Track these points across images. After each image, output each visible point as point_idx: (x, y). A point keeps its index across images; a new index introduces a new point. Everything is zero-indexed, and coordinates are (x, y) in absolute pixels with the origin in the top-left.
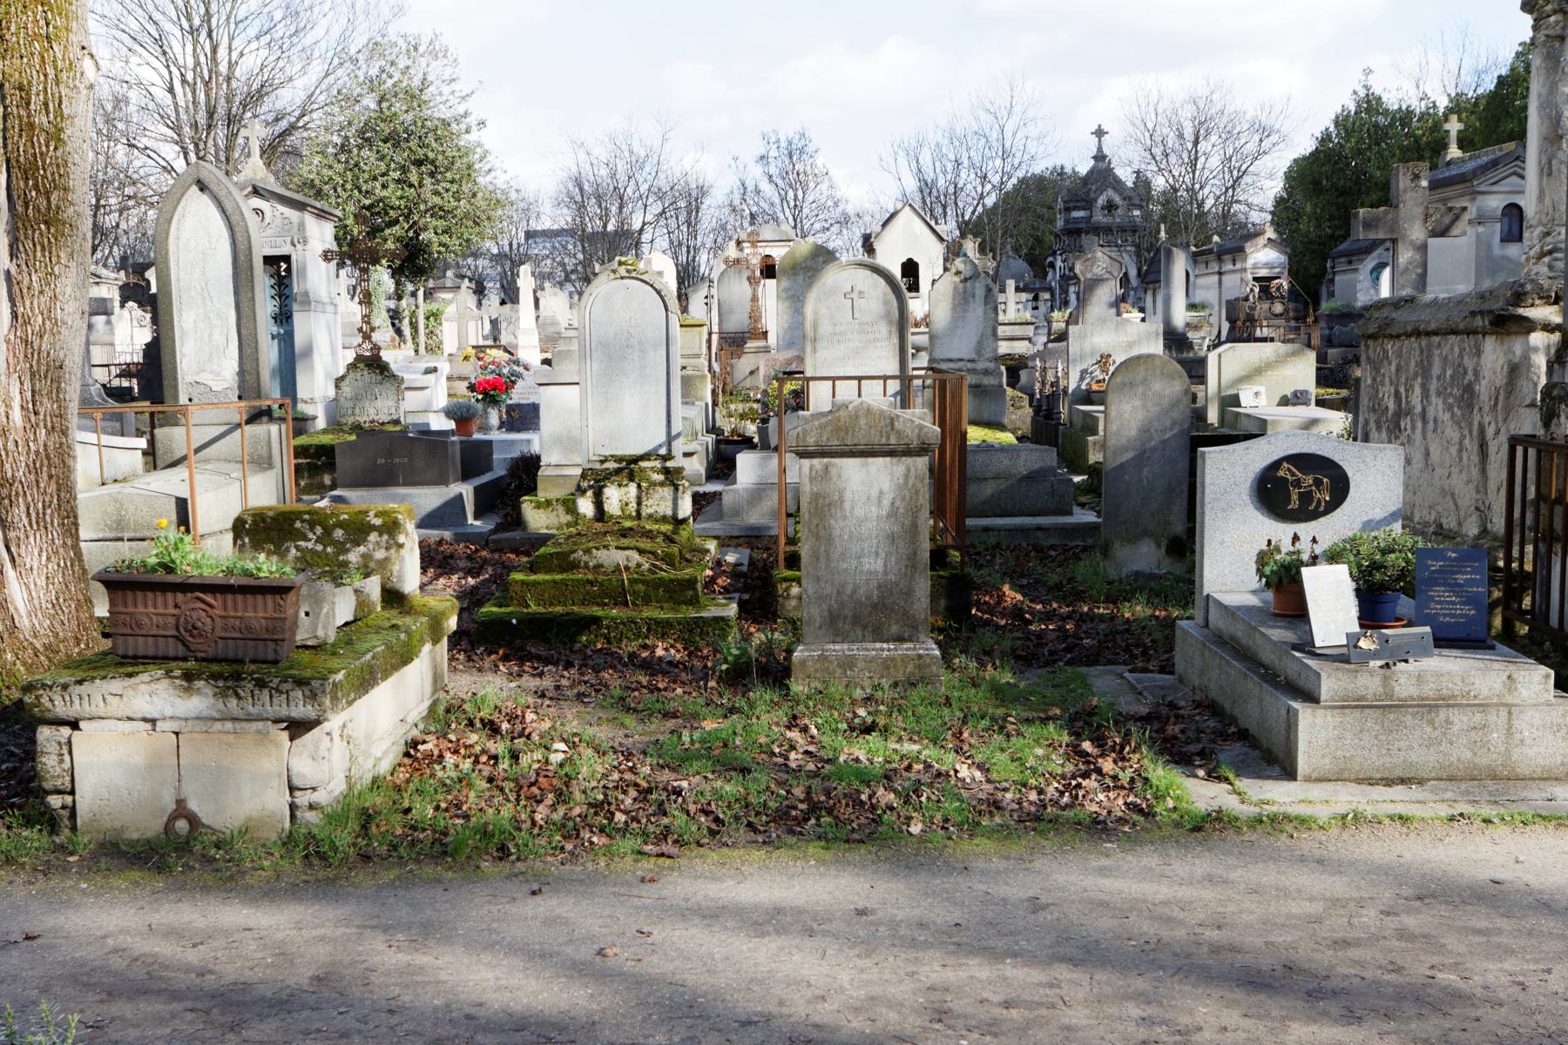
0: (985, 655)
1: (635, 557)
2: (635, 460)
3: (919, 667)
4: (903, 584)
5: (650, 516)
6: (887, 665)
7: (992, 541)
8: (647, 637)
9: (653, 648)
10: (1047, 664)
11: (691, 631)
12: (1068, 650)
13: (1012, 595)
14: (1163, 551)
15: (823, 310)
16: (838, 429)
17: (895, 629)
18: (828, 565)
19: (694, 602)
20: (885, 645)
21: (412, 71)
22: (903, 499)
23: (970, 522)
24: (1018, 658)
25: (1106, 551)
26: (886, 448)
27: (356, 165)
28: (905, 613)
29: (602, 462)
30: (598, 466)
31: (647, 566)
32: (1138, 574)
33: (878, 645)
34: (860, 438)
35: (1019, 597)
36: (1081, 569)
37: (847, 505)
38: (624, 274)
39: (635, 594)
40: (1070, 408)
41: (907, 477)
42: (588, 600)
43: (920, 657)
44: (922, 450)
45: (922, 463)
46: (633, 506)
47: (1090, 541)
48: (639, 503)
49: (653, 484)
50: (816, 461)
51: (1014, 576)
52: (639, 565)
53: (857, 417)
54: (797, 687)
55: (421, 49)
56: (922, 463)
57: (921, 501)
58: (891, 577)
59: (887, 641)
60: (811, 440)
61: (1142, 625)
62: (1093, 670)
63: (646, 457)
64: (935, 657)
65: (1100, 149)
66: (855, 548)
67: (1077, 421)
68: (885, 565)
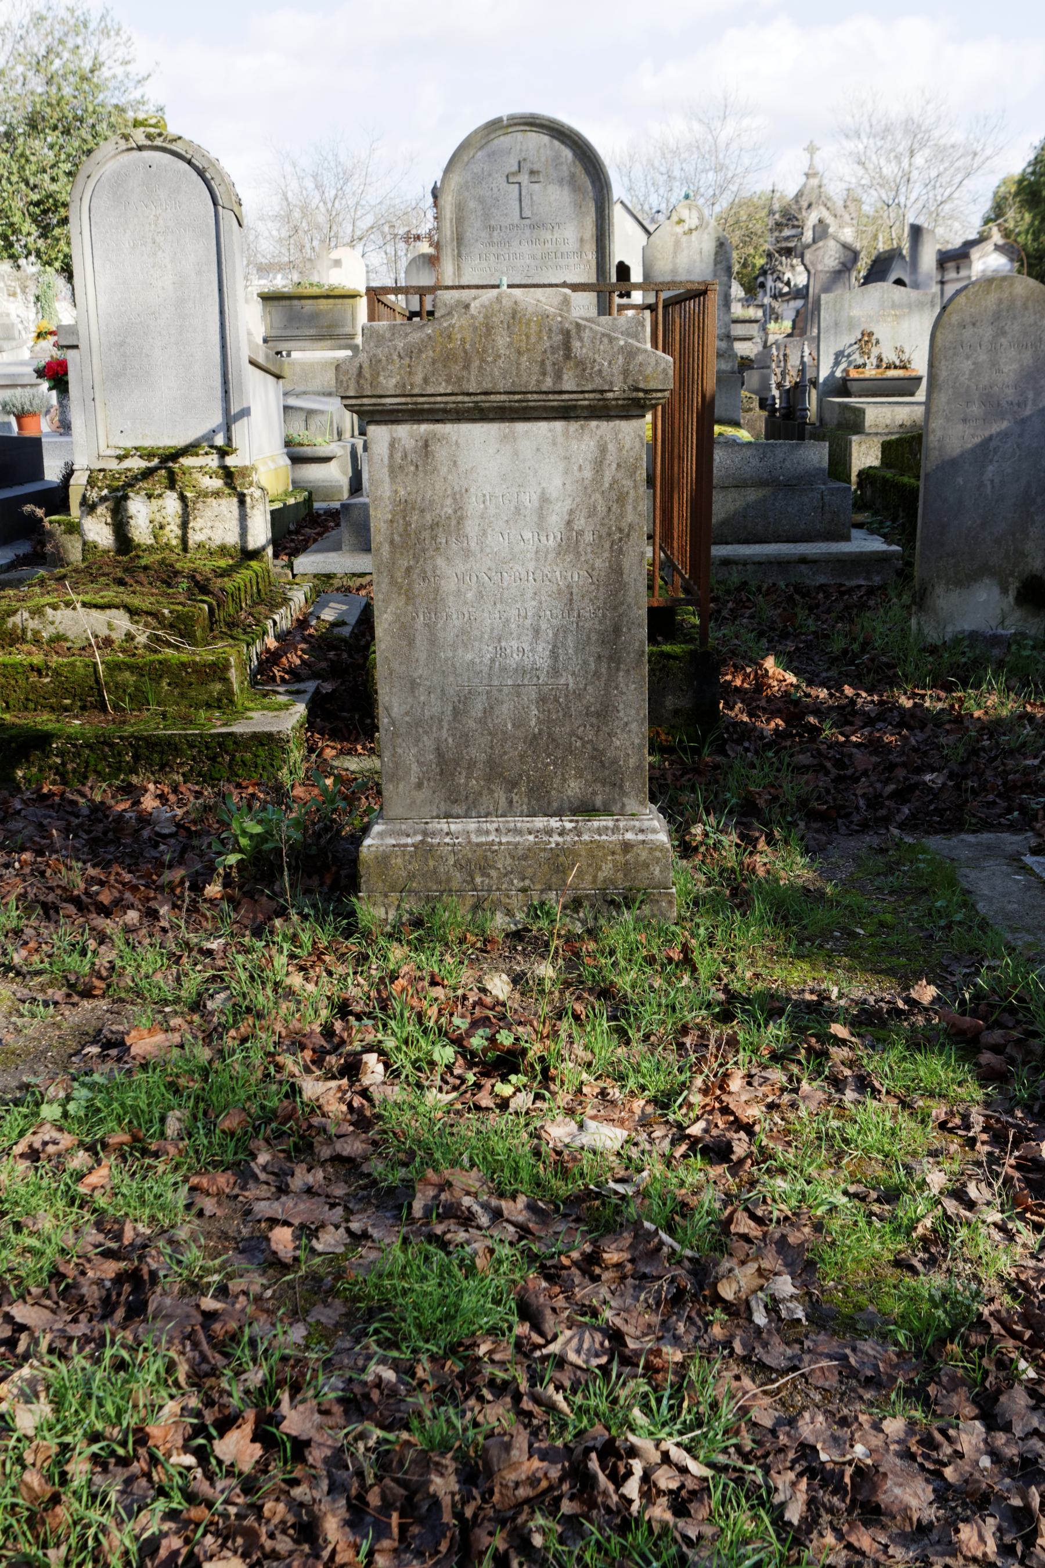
0: (749, 817)
1: (122, 622)
2: (175, 455)
4: (591, 695)
5: (200, 546)
6: (558, 862)
7: (735, 579)
8: (134, 771)
9: (132, 792)
10: (865, 827)
11: (213, 759)
12: (901, 796)
13: (777, 674)
14: (1011, 599)
15: (472, 204)
16: (448, 358)
17: (574, 788)
18: (432, 656)
19: (224, 703)
20: (554, 823)
21: (82, 51)
22: (592, 513)
23: (719, 551)
24: (812, 815)
25: (921, 600)
27: (22, 155)
28: (598, 755)
29: (120, 458)
30: (113, 465)
31: (142, 639)
32: (974, 636)
33: (540, 822)
34: (502, 372)
35: (791, 678)
36: (877, 625)
37: (471, 528)
39: (119, 688)
40: (820, 401)
41: (599, 464)
42: (34, 701)
43: (627, 847)
44: (632, 407)
45: (641, 429)
46: (172, 533)
47: (877, 580)
48: (184, 525)
49: (203, 494)
50: (403, 431)
51: (775, 637)
52: (130, 637)
53: (489, 328)
54: (373, 910)
55: (92, 26)
56: (641, 429)
57: (630, 517)
58: (567, 679)
59: (559, 814)
60: (389, 383)
61: (994, 727)
62: (961, 845)
64: (661, 848)
65: (811, 166)
66: (488, 619)
67: (832, 418)
68: (554, 655)
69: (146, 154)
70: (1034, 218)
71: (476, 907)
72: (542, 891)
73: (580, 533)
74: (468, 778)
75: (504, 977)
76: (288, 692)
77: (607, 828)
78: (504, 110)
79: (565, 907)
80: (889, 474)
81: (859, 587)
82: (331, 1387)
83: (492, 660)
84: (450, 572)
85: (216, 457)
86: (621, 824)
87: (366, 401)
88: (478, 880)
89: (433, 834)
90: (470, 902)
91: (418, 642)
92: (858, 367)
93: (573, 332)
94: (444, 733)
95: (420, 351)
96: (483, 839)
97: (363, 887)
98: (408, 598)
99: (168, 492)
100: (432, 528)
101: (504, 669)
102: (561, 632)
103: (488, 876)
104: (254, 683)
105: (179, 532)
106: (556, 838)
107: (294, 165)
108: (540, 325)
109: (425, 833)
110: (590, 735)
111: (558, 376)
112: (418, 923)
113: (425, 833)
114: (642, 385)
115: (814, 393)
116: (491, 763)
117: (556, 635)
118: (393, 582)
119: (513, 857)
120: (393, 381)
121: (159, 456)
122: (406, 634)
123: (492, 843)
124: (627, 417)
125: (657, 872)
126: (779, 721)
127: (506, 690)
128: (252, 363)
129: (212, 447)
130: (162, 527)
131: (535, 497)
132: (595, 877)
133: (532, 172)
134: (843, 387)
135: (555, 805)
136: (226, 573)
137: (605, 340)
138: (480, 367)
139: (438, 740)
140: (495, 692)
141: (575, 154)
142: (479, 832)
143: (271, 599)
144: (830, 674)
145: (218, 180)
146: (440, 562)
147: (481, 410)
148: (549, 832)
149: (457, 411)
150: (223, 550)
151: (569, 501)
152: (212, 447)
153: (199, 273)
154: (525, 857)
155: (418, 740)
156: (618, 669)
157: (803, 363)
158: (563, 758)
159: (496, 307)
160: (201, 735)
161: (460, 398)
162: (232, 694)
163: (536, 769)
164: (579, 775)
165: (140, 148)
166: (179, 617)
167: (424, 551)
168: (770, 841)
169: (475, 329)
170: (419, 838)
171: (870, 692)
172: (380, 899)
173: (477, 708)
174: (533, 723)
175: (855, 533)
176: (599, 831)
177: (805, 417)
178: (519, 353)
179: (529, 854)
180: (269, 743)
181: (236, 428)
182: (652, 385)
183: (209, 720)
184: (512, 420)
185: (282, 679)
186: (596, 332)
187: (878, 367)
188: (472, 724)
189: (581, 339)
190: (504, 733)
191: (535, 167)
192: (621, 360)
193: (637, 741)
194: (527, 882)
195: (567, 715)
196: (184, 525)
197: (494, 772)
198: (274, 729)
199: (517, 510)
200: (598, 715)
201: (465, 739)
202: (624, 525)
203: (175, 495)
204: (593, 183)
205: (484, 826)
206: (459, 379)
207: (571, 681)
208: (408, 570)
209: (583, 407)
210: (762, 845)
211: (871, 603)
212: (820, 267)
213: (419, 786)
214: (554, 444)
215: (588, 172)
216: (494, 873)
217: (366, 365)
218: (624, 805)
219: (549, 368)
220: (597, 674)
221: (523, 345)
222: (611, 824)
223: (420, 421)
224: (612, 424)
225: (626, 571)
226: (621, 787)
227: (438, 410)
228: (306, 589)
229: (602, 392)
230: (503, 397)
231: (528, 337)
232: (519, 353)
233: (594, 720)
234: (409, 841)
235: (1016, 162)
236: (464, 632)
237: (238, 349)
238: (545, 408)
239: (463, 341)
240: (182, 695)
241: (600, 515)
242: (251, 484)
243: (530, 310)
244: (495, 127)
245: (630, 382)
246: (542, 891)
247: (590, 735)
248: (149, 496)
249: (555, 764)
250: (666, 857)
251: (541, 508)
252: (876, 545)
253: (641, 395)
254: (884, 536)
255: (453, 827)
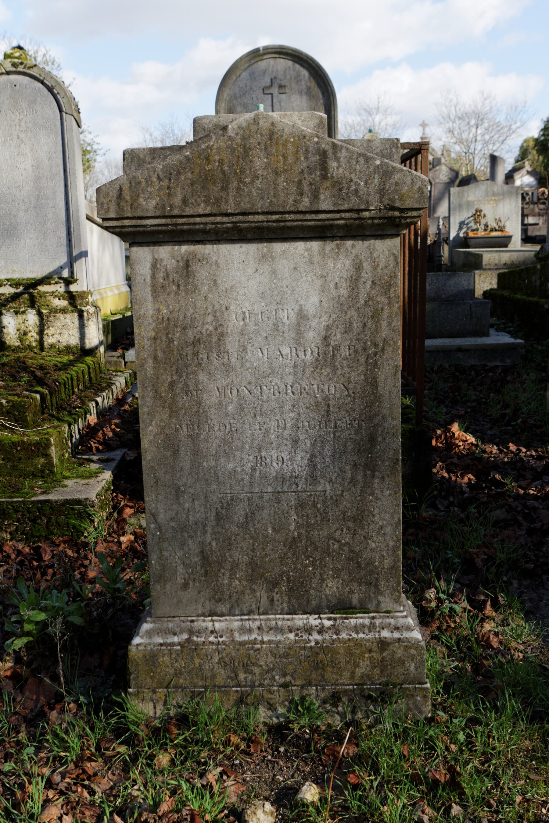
3: (382, 665)
5: (52, 346)
6: (318, 661)
13: (462, 437)
16: (206, 179)
17: (332, 587)
20: (313, 620)
22: (348, 328)
26: (311, 220)
28: (354, 557)
33: (300, 620)
34: (256, 196)
35: (471, 439)
37: (232, 344)
38: (10, 68)
41: (354, 282)
43: (383, 644)
46: (33, 337)
47: (508, 362)
48: (41, 333)
49: (54, 311)
50: (164, 252)
53: (247, 149)
59: (317, 611)
60: (149, 205)
63: (46, 280)
64: (415, 645)
65: (424, 134)
68: (312, 464)
69: (12, 77)
70: (544, 158)
71: (241, 701)
72: (302, 687)
73: (337, 348)
74: (231, 578)
75: (268, 806)
76: (100, 461)
77: (363, 626)
78: (263, 42)
79: (324, 702)
80: (506, 293)
81: (497, 366)
82: (194, 676)
83: (253, 469)
84: (211, 386)
85: (63, 285)
86: (377, 622)
87: (127, 223)
88: (242, 676)
89: (199, 633)
90: (234, 697)
91: (182, 453)
92: (474, 230)
93: (330, 153)
94: (208, 537)
95: (179, 173)
96: (246, 638)
97: (133, 683)
98: (172, 411)
99: (30, 310)
100: (194, 344)
101: (264, 477)
102: (318, 442)
103: (251, 672)
104: (75, 452)
105: (37, 337)
106: (316, 636)
107: (151, 135)
108: (297, 146)
109: (191, 632)
110: (347, 539)
111: (315, 196)
112: (183, 721)
113: (191, 632)
114: (398, 204)
115: (446, 248)
116: (253, 565)
117: (313, 445)
118: (157, 395)
119: (274, 655)
120: (153, 203)
121: (23, 285)
122: (171, 446)
123: (255, 642)
124: (382, 237)
125: (412, 668)
126: (471, 476)
127: (266, 497)
128: (89, 218)
129: (60, 278)
130: (25, 334)
131: (292, 314)
132: (353, 673)
133: (280, 87)
134: (465, 242)
135: (314, 603)
136: (65, 367)
137: (362, 160)
138: (238, 188)
139: (202, 543)
140: (256, 499)
141: (311, 74)
142: (243, 630)
143: (97, 383)
144: (493, 432)
145: (62, 94)
146: (202, 376)
147: (240, 231)
148: (309, 630)
149: (216, 232)
150: (68, 349)
151: (325, 318)
152: (60, 278)
153: (50, 159)
154: (286, 655)
155: (183, 544)
156: (373, 477)
157: (439, 229)
158: (321, 560)
159: (253, 128)
160: (23, 502)
161: (218, 219)
162: (53, 466)
163: (295, 570)
164: (337, 575)
165: (8, 73)
166: (14, 405)
167: (186, 366)
168: (496, 605)
169: (233, 150)
170: (185, 636)
171: (528, 449)
172: (148, 694)
173: (240, 512)
174: (292, 527)
175: (492, 331)
176: (357, 629)
177: (441, 260)
178: (277, 174)
179: (289, 652)
180: (78, 509)
181: (76, 265)
182: (408, 204)
183: (32, 488)
184: (270, 240)
185: (97, 448)
186: (352, 152)
187: (485, 230)
188: (234, 529)
189: (337, 159)
190: (265, 537)
191: (283, 83)
192: (377, 180)
193: (391, 544)
194: (288, 678)
195: (325, 519)
196: (41, 333)
197: (255, 573)
198: (82, 497)
199: (276, 327)
200: (354, 519)
201: (228, 543)
202: (379, 340)
203: (34, 312)
204: (323, 93)
205: (247, 624)
206: (218, 201)
207: (328, 488)
208: (172, 384)
209: (339, 227)
210: (489, 610)
211: (509, 378)
212: (437, 181)
213: (185, 586)
214: (311, 262)
215: (319, 86)
216: (256, 670)
217: (126, 188)
218: (379, 603)
219: (306, 188)
220: (353, 481)
221: (281, 165)
222: (367, 622)
223: (181, 243)
224: (366, 243)
225: (381, 384)
226: (376, 586)
227: (198, 231)
228: (127, 375)
229: (358, 211)
230: (261, 218)
231: (285, 158)
232: (277, 174)
233: (350, 524)
234: (176, 639)
235: (534, 131)
236: (226, 442)
237: (78, 211)
238: (302, 228)
239: (221, 162)
240: (14, 468)
241: (356, 330)
242: (87, 304)
243: (287, 131)
244: (256, 55)
245: (386, 201)
246: (302, 687)
247: (347, 539)
248: (16, 313)
249: (313, 564)
250: (421, 655)
251: (299, 325)
252: (506, 339)
253: (397, 214)
254: (509, 332)
255: (217, 625)
